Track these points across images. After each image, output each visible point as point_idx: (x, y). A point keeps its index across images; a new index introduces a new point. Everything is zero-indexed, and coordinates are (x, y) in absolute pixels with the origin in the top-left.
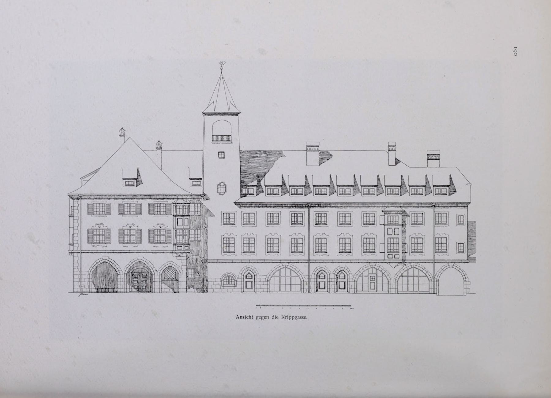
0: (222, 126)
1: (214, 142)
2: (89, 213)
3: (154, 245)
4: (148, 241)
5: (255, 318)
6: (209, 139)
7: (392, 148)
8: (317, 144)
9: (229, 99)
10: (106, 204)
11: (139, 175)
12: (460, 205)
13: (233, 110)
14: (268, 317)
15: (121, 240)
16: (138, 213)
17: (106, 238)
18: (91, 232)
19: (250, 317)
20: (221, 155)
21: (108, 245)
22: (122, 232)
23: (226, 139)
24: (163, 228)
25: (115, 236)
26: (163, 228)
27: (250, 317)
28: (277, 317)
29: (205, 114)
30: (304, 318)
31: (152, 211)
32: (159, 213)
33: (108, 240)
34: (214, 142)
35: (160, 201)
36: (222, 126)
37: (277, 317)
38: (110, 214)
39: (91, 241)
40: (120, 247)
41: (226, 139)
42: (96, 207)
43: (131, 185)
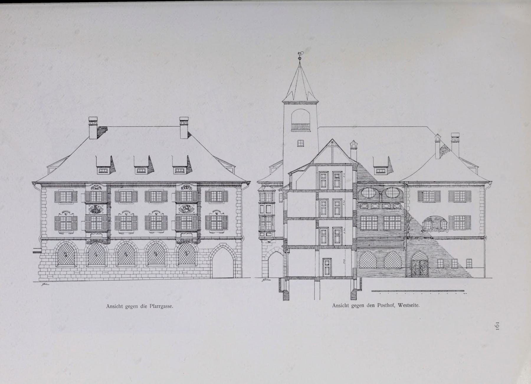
0: (300, 115)
1: (293, 130)
2: (116, 201)
3: (211, 231)
4: (144, 228)
5: (124, 307)
6: (289, 127)
7: (184, 122)
8: (96, 119)
9: (293, 89)
10: (72, 192)
11: (188, 161)
12: (236, 184)
13: (311, 99)
14: (137, 306)
15: (148, 227)
16: (165, 200)
17: (162, 224)
18: (57, 220)
19: (120, 306)
20: (301, 144)
21: (225, 231)
22: (148, 219)
23: (305, 127)
24: (68, 215)
25: (141, 223)
26: (68, 215)
27: (120, 306)
28: (146, 307)
29: (285, 103)
30: (170, 307)
31: (148, 198)
32: (125, 200)
33: (165, 226)
34: (293, 130)
35: (216, 189)
36: (300, 115)
37: (146, 307)
38: (227, 201)
39: (57, 227)
40: (147, 234)
41: (305, 127)
42: (214, 195)
43: (181, 172)
